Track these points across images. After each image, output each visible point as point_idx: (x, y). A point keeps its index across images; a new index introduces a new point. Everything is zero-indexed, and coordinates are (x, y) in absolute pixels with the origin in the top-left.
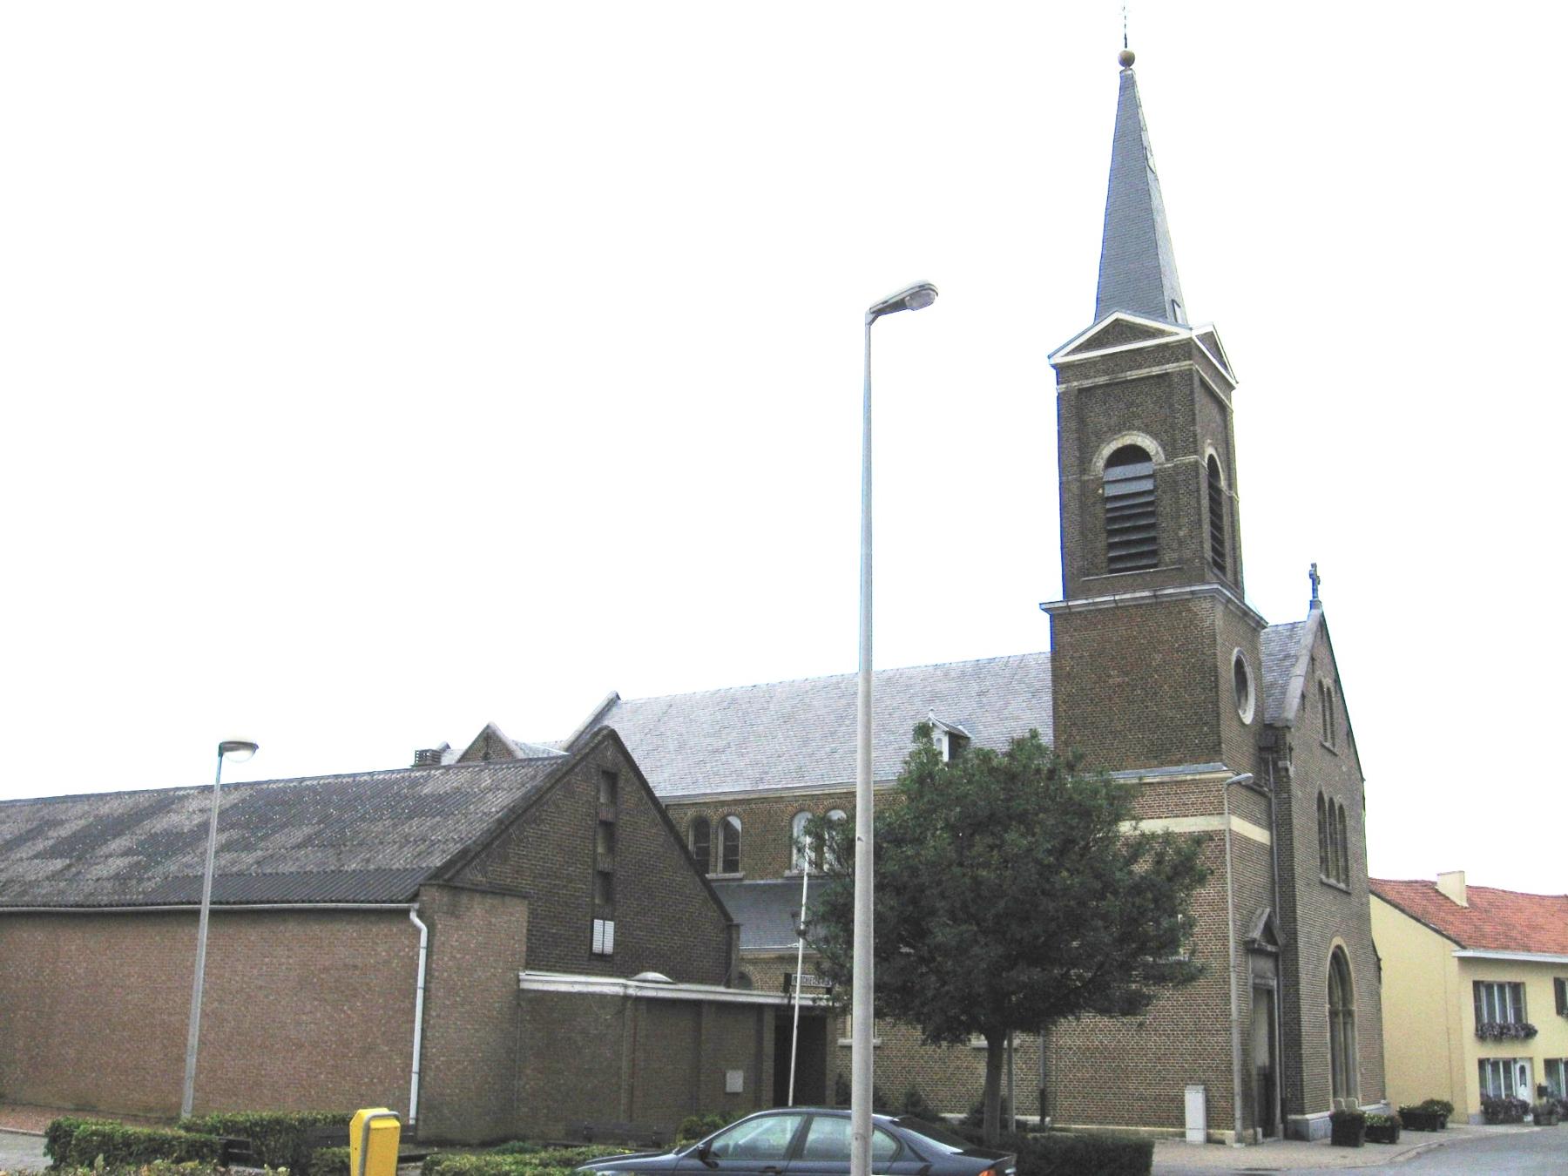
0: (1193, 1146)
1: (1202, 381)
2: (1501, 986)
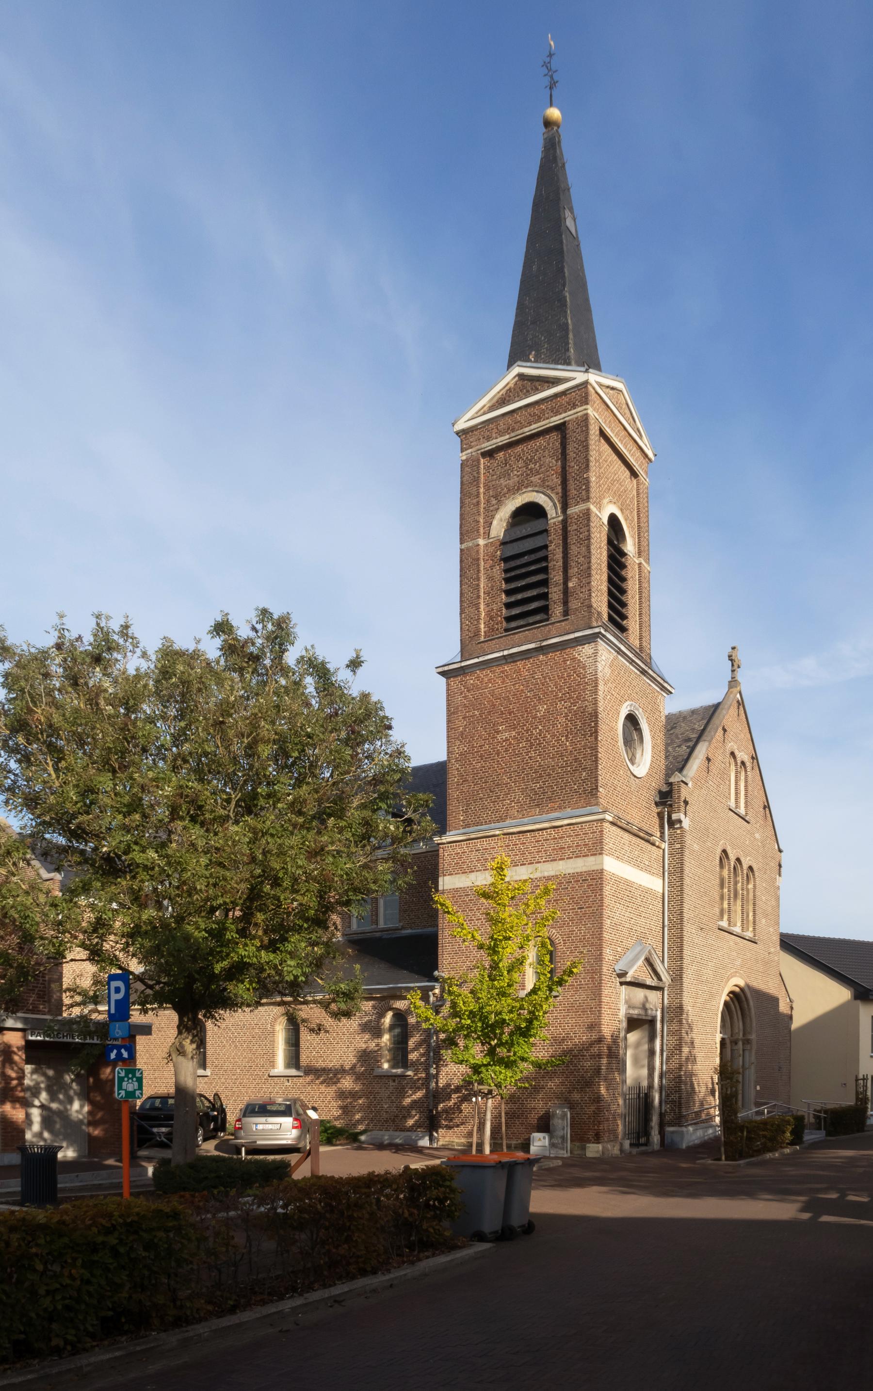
1: (602, 434)
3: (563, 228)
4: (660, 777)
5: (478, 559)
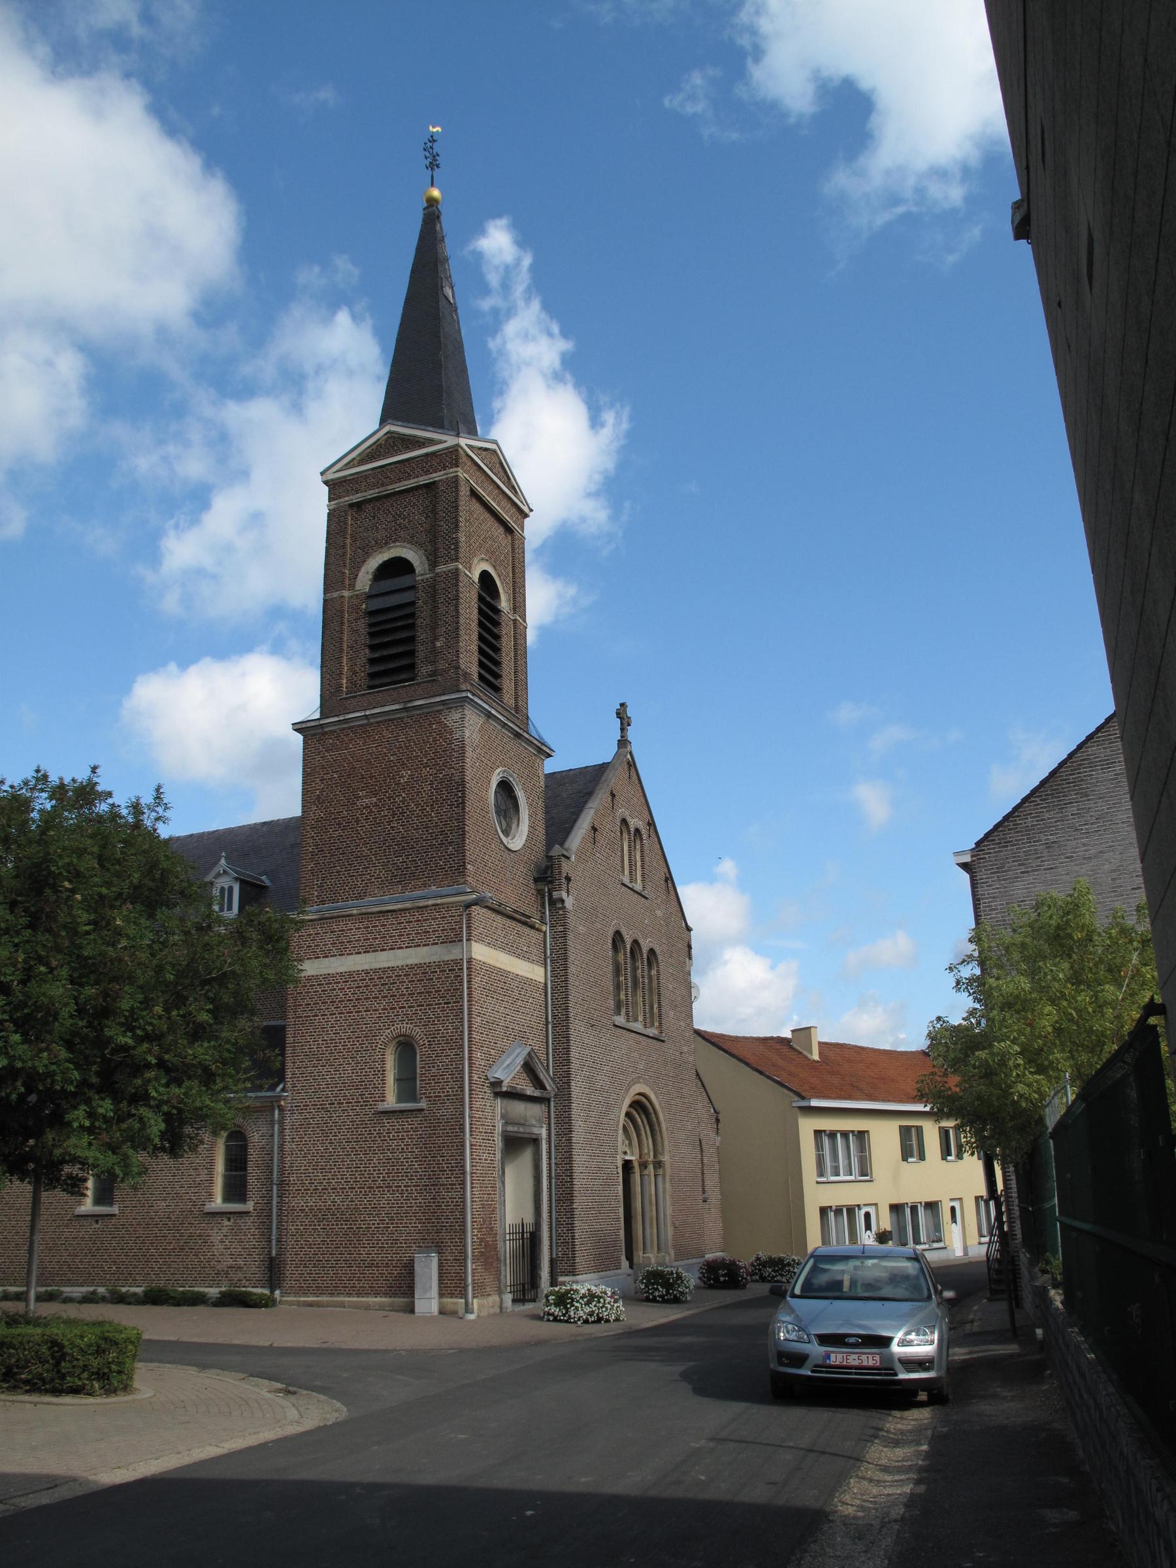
0: (429, 1319)
1: (474, 493)
2: (845, 1134)
3: (441, 296)
4: (540, 847)
5: (342, 612)
